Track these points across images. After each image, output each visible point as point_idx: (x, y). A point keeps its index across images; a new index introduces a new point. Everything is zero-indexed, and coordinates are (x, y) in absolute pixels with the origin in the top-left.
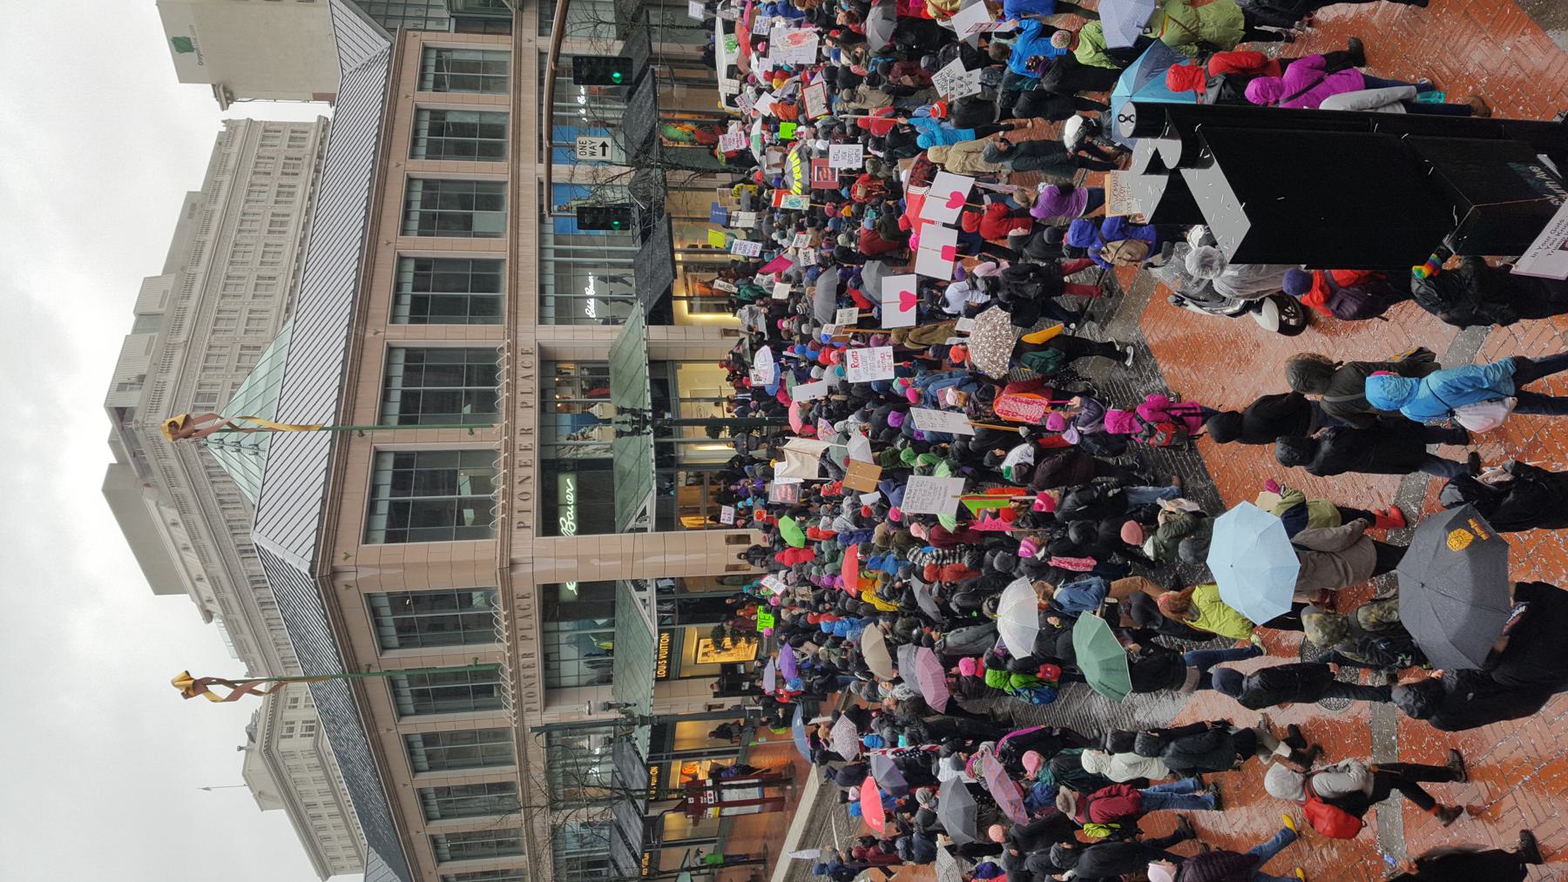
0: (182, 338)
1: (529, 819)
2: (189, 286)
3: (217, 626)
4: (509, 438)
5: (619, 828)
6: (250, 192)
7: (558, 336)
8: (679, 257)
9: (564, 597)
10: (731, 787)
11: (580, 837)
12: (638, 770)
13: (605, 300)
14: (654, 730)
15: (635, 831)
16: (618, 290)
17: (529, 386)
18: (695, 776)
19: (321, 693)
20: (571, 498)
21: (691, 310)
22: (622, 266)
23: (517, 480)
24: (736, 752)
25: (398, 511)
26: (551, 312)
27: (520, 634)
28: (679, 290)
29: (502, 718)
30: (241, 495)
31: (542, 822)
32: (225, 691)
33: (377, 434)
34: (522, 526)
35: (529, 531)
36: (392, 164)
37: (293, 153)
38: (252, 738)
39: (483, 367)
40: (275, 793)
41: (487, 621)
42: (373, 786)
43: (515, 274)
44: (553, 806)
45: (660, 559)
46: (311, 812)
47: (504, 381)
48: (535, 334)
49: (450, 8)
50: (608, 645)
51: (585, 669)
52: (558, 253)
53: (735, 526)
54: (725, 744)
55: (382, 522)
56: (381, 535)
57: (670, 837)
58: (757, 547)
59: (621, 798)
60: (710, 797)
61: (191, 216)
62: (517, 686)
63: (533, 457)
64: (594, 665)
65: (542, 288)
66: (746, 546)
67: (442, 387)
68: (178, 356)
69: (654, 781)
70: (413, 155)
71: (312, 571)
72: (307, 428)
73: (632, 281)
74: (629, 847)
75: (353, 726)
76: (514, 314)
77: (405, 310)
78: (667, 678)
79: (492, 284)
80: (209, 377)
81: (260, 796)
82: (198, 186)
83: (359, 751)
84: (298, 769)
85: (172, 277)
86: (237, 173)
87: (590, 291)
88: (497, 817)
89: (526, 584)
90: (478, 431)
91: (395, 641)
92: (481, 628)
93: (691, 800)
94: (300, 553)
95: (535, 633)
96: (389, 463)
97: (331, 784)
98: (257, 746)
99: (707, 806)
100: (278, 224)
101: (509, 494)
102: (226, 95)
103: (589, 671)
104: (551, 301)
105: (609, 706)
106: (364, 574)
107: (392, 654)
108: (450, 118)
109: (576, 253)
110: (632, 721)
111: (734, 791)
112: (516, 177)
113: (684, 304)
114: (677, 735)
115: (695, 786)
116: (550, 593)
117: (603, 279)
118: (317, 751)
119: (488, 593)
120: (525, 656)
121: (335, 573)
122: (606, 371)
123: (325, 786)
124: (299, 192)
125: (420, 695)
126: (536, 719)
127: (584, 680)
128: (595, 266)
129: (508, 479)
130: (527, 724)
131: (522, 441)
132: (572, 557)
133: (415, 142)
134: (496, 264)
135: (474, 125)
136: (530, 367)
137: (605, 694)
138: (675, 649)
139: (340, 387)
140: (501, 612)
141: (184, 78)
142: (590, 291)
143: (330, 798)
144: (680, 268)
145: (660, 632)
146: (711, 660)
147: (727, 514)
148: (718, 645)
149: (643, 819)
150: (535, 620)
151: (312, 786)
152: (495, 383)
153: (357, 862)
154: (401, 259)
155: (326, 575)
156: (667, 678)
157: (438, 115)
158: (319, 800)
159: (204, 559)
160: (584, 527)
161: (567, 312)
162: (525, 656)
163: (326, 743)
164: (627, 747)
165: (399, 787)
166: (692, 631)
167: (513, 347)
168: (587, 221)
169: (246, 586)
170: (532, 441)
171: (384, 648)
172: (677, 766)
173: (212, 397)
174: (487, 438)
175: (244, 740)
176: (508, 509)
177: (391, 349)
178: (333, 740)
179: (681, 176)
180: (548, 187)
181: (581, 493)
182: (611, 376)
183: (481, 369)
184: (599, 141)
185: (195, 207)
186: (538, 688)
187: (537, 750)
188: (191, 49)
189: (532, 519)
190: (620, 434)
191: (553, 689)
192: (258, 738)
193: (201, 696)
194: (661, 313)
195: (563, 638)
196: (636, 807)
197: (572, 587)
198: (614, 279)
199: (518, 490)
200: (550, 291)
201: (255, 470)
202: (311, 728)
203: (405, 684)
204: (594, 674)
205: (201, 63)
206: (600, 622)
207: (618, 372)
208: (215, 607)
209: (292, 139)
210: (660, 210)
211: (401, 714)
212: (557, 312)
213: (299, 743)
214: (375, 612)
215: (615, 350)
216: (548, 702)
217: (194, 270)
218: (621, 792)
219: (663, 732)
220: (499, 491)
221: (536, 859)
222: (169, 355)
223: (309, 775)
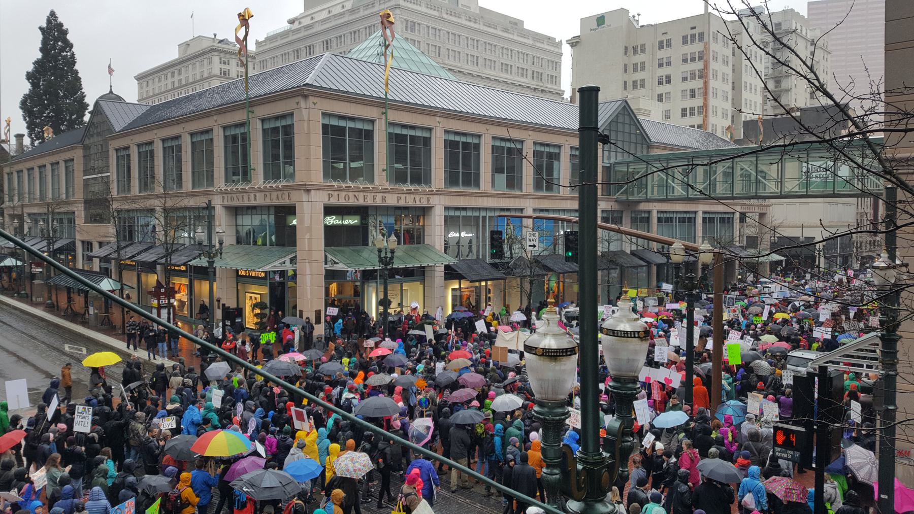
0: (445, 16)
1: (158, 196)
2: (473, 21)
3: (285, 26)
4: (380, 189)
5: (151, 248)
6: (523, 54)
7: (438, 217)
8: (483, 283)
9: (289, 218)
10: (169, 314)
11: (147, 225)
12: (184, 259)
13: (458, 243)
14: (206, 268)
15: (148, 257)
16: (465, 250)
17: (409, 201)
18: (179, 292)
19: (239, 85)
20: (346, 222)
21: (453, 290)
22: (478, 251)
23: (356, 194)
24: (191, 316)
25: (340, 131)
26: (452, 213)
27: (268, 194)
28: (465, 284)
29: (220, 183)
30: (359, 43)
31: (156, 203)
32: (241, 35)
33: (383, 121)
34: (330, 196)
35: (327, 200)
36: (530, 133)
37: (545, 77)
38: (221, 41)
39: (420, 176)
40: (189, 52)
41: (277, 177)
42: (185, 110)
43: (471, 195)
44: (166, 210)
45: (308, 272)
46: (176, 72)
47: (412, 188)
48: (439, 206)
49: (616, 163)
50: (260, 242)
51: (246, 229)
52: (484, 218)
53: (326, 316)
54: (196, 310)
55: (334, 122)
56: (326, 122)
57: (143, 277)
58: (313, 328)
59: (167, 250)
60: (164, 301)
61: (510, 22)
62: (237, 192)
63: (369, 202)
64: (248, 234)
65: (464, 209)
66: (314, 322)
67: (409, 153)
68: (436, 13)
69: (177, 268)
70: (535, 143)
71: (307, 84)
72: (387, 85)
73: (470, 257)
74: (138, 254)
75: (219, 102)
76: (450, 194)
77: (452, 138)
78: (238, 276)
79: (467, 183)
80: (424, 28)
81: (187, 44)
82: (526, 26)
83: (205, 104)
84: (202, 66)
85: (478, 12)
86: (533, 47)
87: (463, 234)
88: (161, 179)
89: (296, 198)
90: (384, 173)
91: (267, 126)
92: (272, 172)
93: (163, 290)
94: (318, 79)
95: (268, 202)
96: (367, 127)
97: (192, 83)
98: (216, 44)
99: (159, 299)
100: (507, 68)
101: (348, 189)
102: (574, 43)
103: (245, 231)
104: (457, 213)
105: (221, 243)
106: (305, 112)
107: (259, 125)
108: (556, 163)
109: (484, 228)
110: (211, 257)
111: (166, 315)
112: (525, 197)
113: (457, 286)
114: (203, 282)
115: (171, 292)
116: (291, 210)
117: (470, 242)
118: (211, 76)
119: (292, 176)
120: (255, 196)
121: (306, 97)
122: (419, 243)
123: (191, 80)
124: (524, 80)
125: (234, 138)
126: (217, 202)
127: (240, 228)
128: (478, 238)
129: (357, 190)
130: (215, 197)
131: (379, 197)
132: (311, 222)
133: (542, 144)
134: (477, 185)
135: (552, 175)
136: (421, 201)
137: (229, 239)
138: (256, 280)
139: (409, 103)
140: (281, 184)
141: (583, 21)
142: (463, 234)
143: (183, 83)
144: (477, 284)
145: (266, 272)
146: (247, 301)
147: (333, 311)
148: (255, 306)
149: (155, 261)
150: (276, 202)
151: (191, 73)
152: (411, 183)
153: (145, 96)
154: (479, 136)
155: (303, 92)
156: (238, 276)
157: (557, 157)
158: (183, 77)
159: (323, 21)
160: (328, 229)
161: (450, 222)
162: (255, 196)
163: (216, 83)
164: (197, 252)
165: (183, 125)
166: (265, 290)
167: (431, 193)
168: (495, 236)
169: (308, 43)
170: (379, 202)
171: (263, 121)
172: (185, 281)
173: (413, 30)
174: (381, 178)
175: (220, 37)
176: (340, 189)
177: (430, 130)
178: (213, 90)
179: (527, 286)
180: (518, 216)
181: (349, 227)
182: (416, 246)
183: (420, 176)
184: (536, 243)
185: (515, 25)
186: (236, 203)
187: (201, 202)
188: (598, 25)
189: (334, 201)
190: (380, 251)
191: (235, 211)
192: (220, 45)
193: (239, 23)
194: (451, 273)
195: (265, 217)
196: (162, 258)
197: (294, 222)
198: (470, 247)
199: (351, 194)
200: (463, 213)
201: (369, 53)
202: (225, 74)
203: (242, 131)
204: (243, 233)
205: (591, 30)
206: (273, 238)
207: (418, 249)
208: (296, 26)
209: (552, 76)
210: (509, 274)
211: (225, 128)
212: (452, 217)
213: (216, 66)
214: (283, 117)
215: (430, 248)
216: (228, 208)
217: (482, 23)
218: (170, 249)
219: (206, 273)
220: (350, 184)
221: (135, 199)
222: (436, 8)
223: (190, 74)
